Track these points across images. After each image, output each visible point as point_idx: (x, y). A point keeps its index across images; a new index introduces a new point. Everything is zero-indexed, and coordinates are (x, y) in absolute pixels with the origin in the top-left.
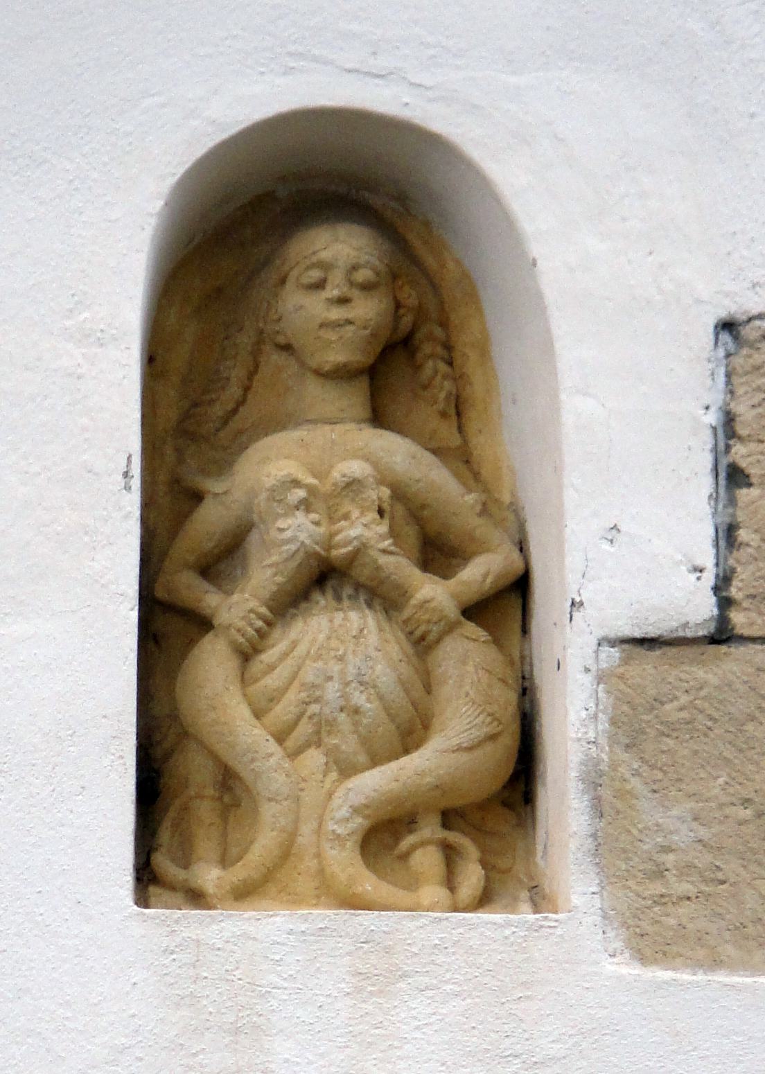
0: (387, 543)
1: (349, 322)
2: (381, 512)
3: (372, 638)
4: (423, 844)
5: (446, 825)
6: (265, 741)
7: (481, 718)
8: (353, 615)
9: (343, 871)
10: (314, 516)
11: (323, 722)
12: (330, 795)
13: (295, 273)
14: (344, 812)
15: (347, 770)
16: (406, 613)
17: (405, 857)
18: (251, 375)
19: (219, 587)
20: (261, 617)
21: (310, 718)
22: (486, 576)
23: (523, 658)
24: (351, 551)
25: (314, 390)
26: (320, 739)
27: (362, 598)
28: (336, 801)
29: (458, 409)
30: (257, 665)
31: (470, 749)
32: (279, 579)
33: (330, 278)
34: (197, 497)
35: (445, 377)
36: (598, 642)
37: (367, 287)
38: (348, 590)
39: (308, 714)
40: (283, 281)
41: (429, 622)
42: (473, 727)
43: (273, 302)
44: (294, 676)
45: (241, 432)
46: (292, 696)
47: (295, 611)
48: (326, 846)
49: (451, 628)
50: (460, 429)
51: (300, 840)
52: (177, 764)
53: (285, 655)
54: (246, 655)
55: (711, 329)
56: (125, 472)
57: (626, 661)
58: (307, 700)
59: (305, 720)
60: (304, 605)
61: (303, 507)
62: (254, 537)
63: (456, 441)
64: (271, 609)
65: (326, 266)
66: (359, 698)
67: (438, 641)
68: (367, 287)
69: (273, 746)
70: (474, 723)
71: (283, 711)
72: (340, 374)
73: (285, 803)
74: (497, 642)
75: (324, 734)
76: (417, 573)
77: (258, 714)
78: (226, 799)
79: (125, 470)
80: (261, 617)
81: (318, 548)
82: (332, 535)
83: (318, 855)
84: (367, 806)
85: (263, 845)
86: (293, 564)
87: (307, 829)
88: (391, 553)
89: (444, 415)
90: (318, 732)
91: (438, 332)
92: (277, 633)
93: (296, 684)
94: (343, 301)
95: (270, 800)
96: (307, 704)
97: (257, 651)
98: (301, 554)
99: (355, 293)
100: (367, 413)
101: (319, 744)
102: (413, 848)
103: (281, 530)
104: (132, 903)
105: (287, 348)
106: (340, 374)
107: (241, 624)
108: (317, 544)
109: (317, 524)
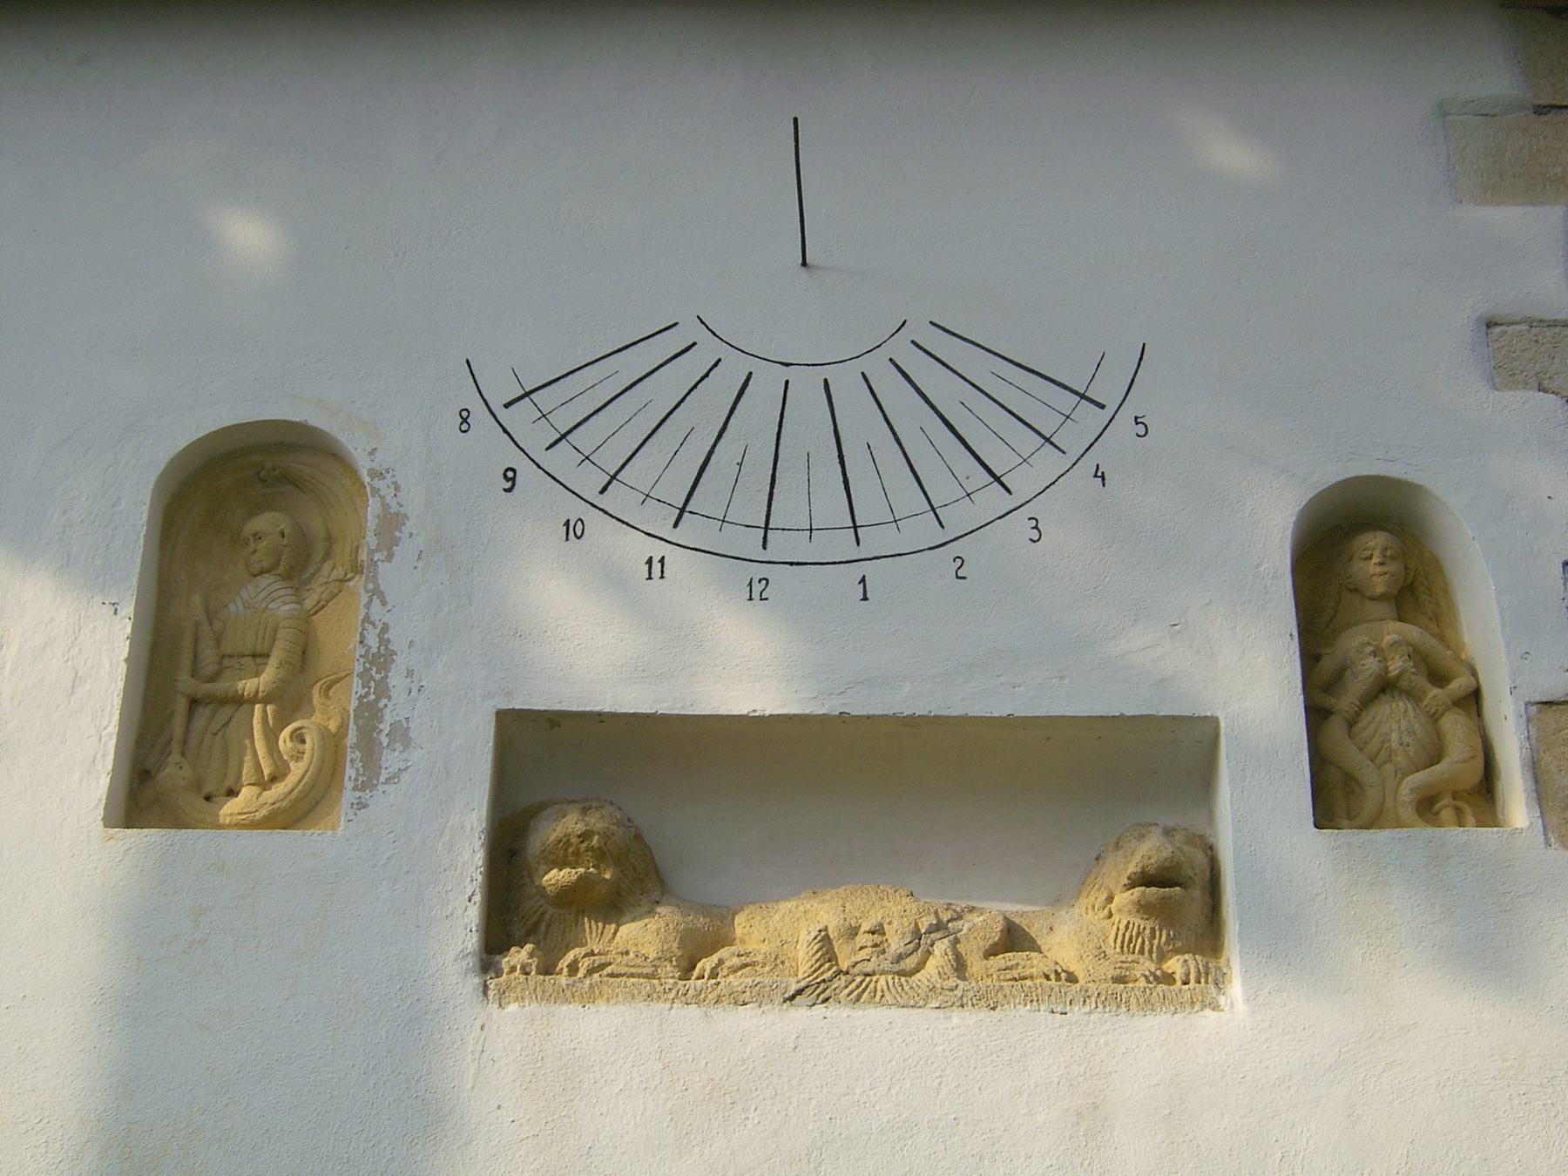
0: (1414, 670)
1: (1385, 574)
2: (1409, 656)
3: (1411, 712)
4: (1448, 806)
5: (1454, 799)
7: (1467, 748)
8: (1401, 704)
10: (1377, 658)
12: (1399, 784)
13: (1357, 554)
14: (1407, 791)
15: (1405, 775)
16: (1426, 702)
17: (1437, 814)
21: (1386, 749)
22: (1460, 686)
25: (1372, 609)
27: (1403, 697)
28: (1402, 787)
29: (1436, 618)
30: (1356, 729)
31: (1463, 762)
32: (1364, 687)
33: (1374, 554)
34: (1318, 658)
37: (1392, 558)
38: (1396, 693)
40: (1350, 559)
41: (1437, 706)
44: (1375, 732)
49: (1447, 710)
52: (1565, 258)
53: (1370, 722)
54: (1351, 724)
55: (1561, 565)
57: (1539, 712)
59: (1384, 750)
60: (1376, 701)
62: (1348, 673)
63: (1438, 631)
64: (1361, 703)
66: (1406, 739)
67: (1443, 714)
68: (1392, 558)
69: (1370, 763)
71: (1373, 746)
72: (1381, 598)
75: (1393, 757)
76: (1429, 686)
77: (1361, 750)
81: (1382, 673)
82: (1387, 668)
85: (1370, 806)
86: (1371, 680)
89: (1431, 619)
90: (1391, 755)
91: (1425, 582)
92: (1364, 714)
94: (1381, 564)
95: (1370, 786)
99: (1388, 561)
100: (1396, 616)
101: (1391, 761)
102: (1441, 809)
103: (1363, 665)
105: (1356, 590)
106: (1381, 598)
107: (1347, 709)
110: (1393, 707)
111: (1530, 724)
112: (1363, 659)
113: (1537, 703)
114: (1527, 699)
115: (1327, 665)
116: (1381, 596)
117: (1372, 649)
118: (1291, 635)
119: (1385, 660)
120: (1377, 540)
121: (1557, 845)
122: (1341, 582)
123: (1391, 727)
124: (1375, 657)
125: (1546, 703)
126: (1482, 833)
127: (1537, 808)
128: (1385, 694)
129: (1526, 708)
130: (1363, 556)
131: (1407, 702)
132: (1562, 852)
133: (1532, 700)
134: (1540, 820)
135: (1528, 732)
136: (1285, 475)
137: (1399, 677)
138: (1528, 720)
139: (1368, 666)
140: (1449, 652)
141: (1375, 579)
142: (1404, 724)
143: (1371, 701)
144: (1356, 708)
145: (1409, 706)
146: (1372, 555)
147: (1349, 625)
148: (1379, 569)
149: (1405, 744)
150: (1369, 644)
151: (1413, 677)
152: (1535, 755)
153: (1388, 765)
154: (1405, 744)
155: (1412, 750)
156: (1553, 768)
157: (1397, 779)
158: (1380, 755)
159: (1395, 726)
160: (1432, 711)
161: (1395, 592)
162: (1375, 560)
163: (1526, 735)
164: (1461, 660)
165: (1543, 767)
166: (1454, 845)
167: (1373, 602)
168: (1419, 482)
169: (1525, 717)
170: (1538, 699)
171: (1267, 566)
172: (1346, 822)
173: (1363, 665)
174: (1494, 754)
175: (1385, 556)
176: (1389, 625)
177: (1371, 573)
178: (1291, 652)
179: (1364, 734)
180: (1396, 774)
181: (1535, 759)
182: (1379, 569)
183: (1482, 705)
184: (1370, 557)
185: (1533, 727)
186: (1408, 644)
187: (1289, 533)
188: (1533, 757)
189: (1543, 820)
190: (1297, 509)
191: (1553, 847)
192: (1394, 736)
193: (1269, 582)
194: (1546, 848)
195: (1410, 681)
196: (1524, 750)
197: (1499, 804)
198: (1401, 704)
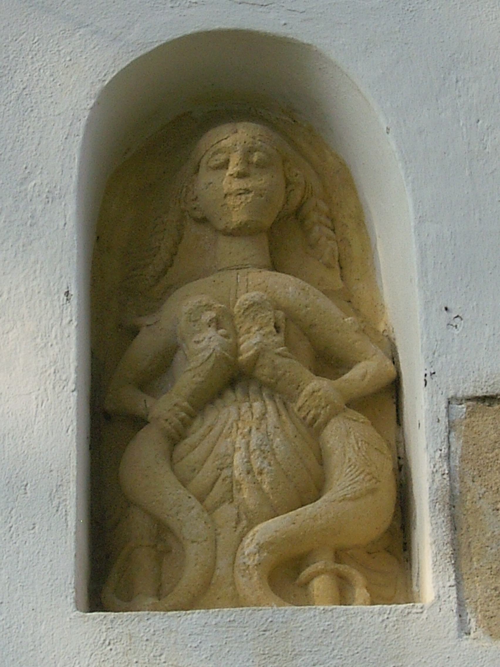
1: (247, 191)
2: (277, 328)
3: (272, 418)
4: (318, 574)
6: (187, 498)
9: (252, 593)
10: (221, 331)
11: (234, 482)
12: (241, 539)
13: (204, 161)
16: (299, 403)
17: (306, 584)
18: (176, 244)
19: (153, 396)
20: (183, 409)
21: (224, 480)
22: (364, 376)
23: (398, 442)
24: (252, 355)
26: (232, 497)
30: (182, 447)
31: (354, 499)
34: (135, 332)
35: (329, 238)
36: (447, 400)
37: (261, 166)
38: (253, 388)
39: (223, 476)
41: (317, 407)
42: (355, 483)
43: (190, 186)
45: (170, 287)
46: (210, 466)
47: (212, 406)
48: (238, 574)
49: (334, 413)
50: (342, 277)
51: (218, 572)
53: (204, 436)
56: (66, 292)
57: (471, 414)
58: (221, 466)
59: (220, 481)
60: (218, 401)
61: (213, 324)
62: (179, 357)
63: (339, 284)
65: (230, 151)
68: (261, 166)
69: (194, 502)
70: (356, 479)
73: (205, 544)
74: (375, 423)
76: (308, 373)
77: (184, 483)
78: (159, 546)
79: (66, 290)
80: (183, 409)
82: (237, 346)
83: (233, 583)
84: (271, 543)
86: (209, 366)
87: (222, 564)
88: (286, 357)
89: (329, 266)
92: (197, 423)
93: (213, 455)
94: (241, 175)
96: (221, 470)
97: (182, 437)
98: (212, 359)
102: (312, 577)
103: (198, 342)
104: (72, 607)
105: (204, 221)
108: (226, 351)
109: (226, 336)
110: (243, 410)
111: (453, 434)
112: (200, 331)
113: (468, 399)
114: (451, 394)
115: (231, 485)
116: (239, 229)
117: (213, 314)
118: (67, 293)
119: (237, 335)
120: (238, 136)
121: (480, 632)
122: (182, 206)
123: (234, 443)
124: (218, 328)
125: (484, 399)
126: (356, 614)
127: (451, 569)
128: (234, 390)
129: (447, 408)
130: (213, 163)
131: (267, 402)
132: (486, 643)
133: (460, 395)
134: (453, 592)
135: (449, 447)
136: (82, 31)
137: (257, 356)
138: (451, 427)
139: (204, 344)
140: (349, 320)
141: (231, 201)
142: (255, 439)
143: (211, 401)
144: (183, 414)
145: (270, 408)
146: (228, 161)
147: (193, 277)
148: (237, 185)
149: (256, 471)
150: (209, 307)
151: (278, 361)
152: (457, 485)
153: (226, 506)
154: (256, 471)
155: (267, 480)
156: (485, 505)
157: (240, 529)
158: (216, 489)
159: (240, 442)
160: (310, 417)
161: (267, 222)
162: (233, 169)
163: (445, 451)
164: (377, 332)
165: (468, 504)
166: (306, 634)
167: (229, 238)
168: (306, 40)
169: (444, 421)
170: (470, 392)
171: (38, 181)
172: (151, 600)
173: (198, 342)
174: (411, 480)
175: (249, 163)
176: (250, 276)
177: (225, 191)
178: (66, 321)
179: (191, 456)
180: (238, 522)
181: (457, 492)
182: (237, 185)
183: (402, 403)
184: (225, 165)
185: (458, 438)
186: (277, 308)
187: (81, 126)
188: (452, 489)
189: (458, 591)
190: (99, 87)
191: (472, 635)
192: (238, 459)
193: (40, 207)
194: (460, 637)
195: (274, 368)
196: (438, 477)
197: (415, 566)
198: (257, 406)
